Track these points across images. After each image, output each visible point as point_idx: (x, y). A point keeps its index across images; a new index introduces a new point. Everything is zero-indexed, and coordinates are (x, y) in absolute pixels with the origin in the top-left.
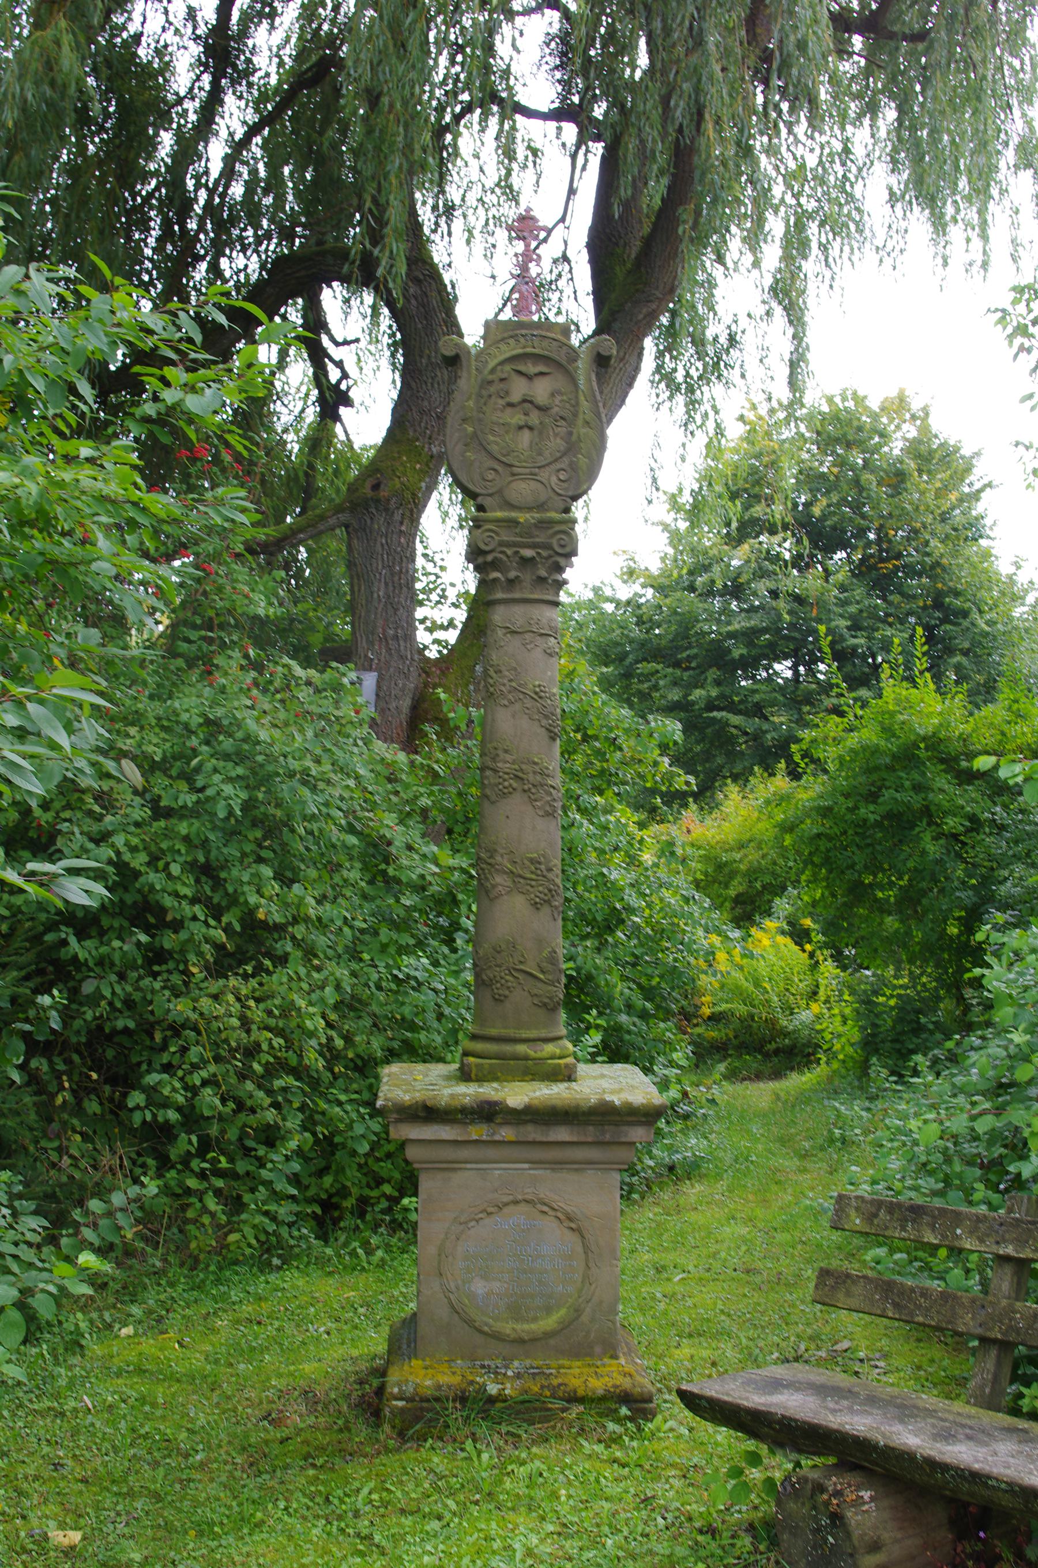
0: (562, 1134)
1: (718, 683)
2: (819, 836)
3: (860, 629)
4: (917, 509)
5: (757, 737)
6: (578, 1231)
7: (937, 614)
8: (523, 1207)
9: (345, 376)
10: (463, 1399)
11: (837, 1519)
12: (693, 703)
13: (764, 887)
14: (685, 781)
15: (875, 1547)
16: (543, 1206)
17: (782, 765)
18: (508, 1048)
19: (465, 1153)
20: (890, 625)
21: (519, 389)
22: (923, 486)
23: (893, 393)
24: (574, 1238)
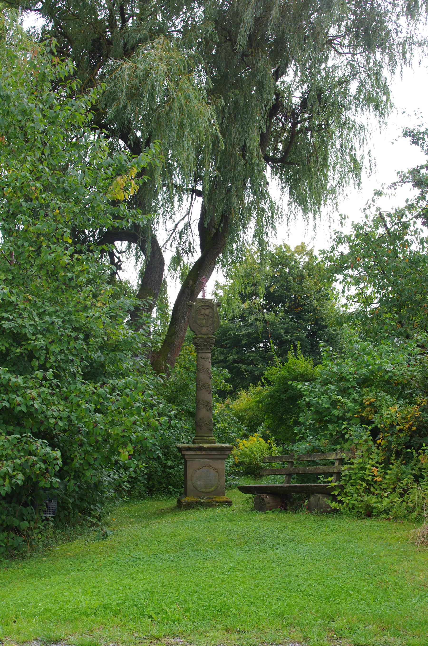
0: (214, 453)
1: (237, 353)
2: (269, 404)
3: (288, 333)
4: (308, 289)
5: (252, 372)
6: (217, 472)
7: (316, 327)
8: (207, 467)
9: (120, 261)
10: (196, 503)
11: (263, 499)
12: (228, 361)
13: (254, 424)
14: (229, 387)
15: (269, 503)
16: (210, 467)
17: (260, 383)
18: (203, 438)
19: (196, 457)
20: (299, 331)
21: (203, 312)
22: (310, 281)
23: (299, 244)
24: (216, 473)
